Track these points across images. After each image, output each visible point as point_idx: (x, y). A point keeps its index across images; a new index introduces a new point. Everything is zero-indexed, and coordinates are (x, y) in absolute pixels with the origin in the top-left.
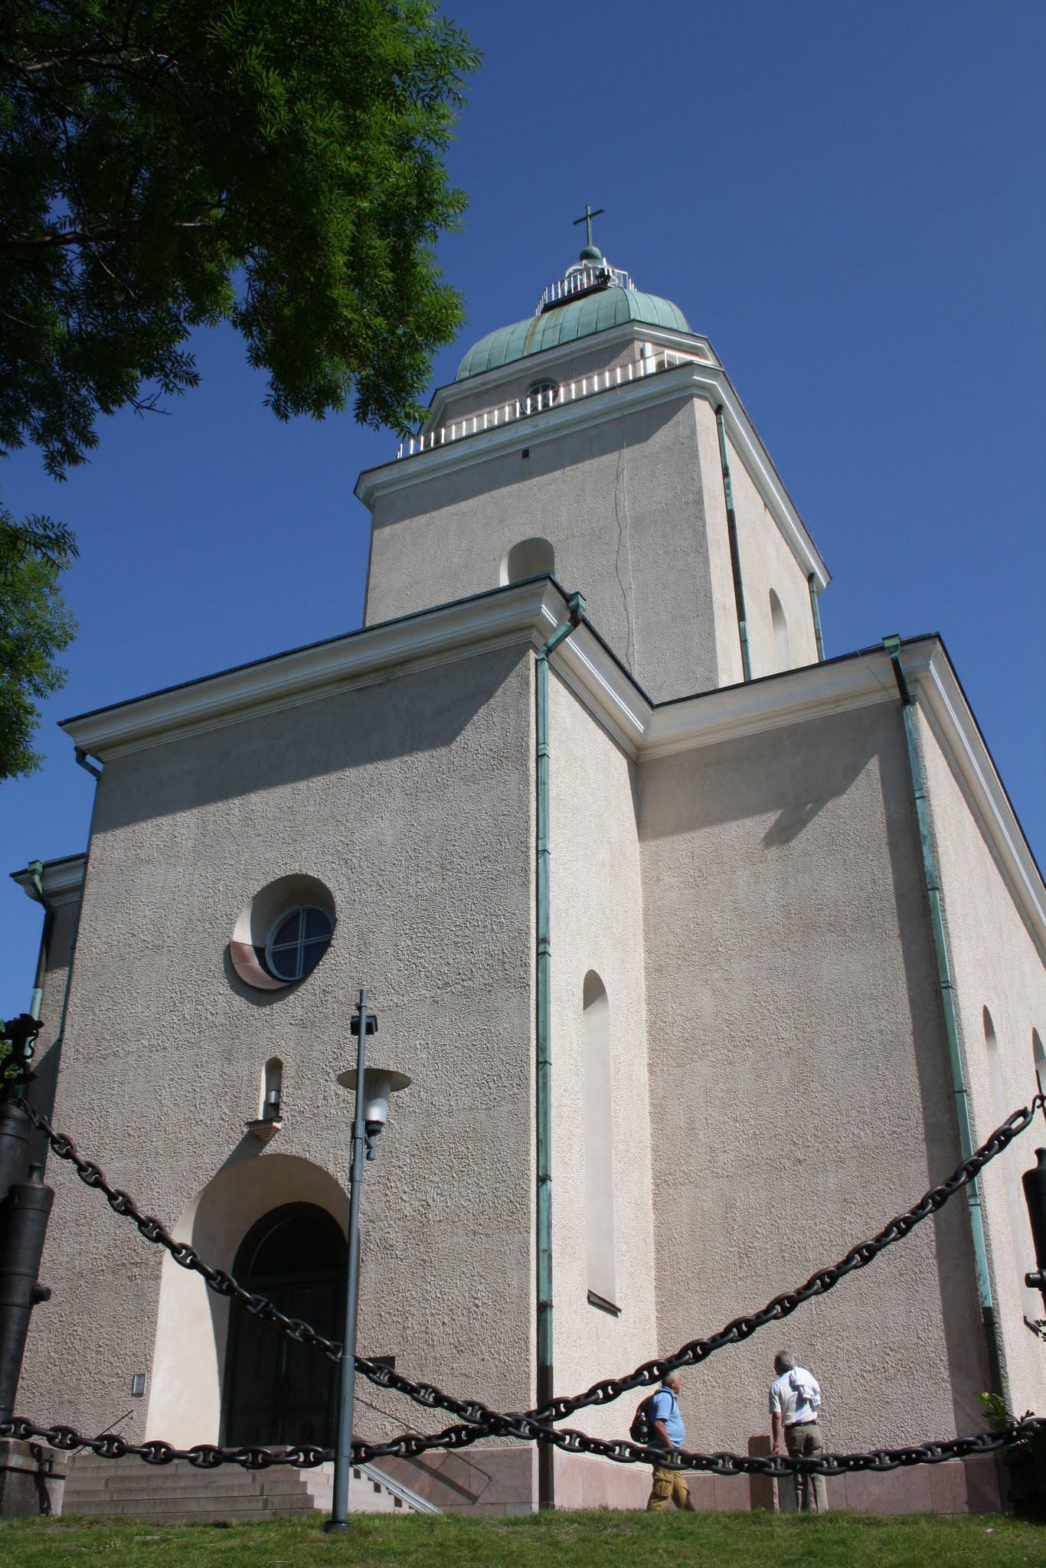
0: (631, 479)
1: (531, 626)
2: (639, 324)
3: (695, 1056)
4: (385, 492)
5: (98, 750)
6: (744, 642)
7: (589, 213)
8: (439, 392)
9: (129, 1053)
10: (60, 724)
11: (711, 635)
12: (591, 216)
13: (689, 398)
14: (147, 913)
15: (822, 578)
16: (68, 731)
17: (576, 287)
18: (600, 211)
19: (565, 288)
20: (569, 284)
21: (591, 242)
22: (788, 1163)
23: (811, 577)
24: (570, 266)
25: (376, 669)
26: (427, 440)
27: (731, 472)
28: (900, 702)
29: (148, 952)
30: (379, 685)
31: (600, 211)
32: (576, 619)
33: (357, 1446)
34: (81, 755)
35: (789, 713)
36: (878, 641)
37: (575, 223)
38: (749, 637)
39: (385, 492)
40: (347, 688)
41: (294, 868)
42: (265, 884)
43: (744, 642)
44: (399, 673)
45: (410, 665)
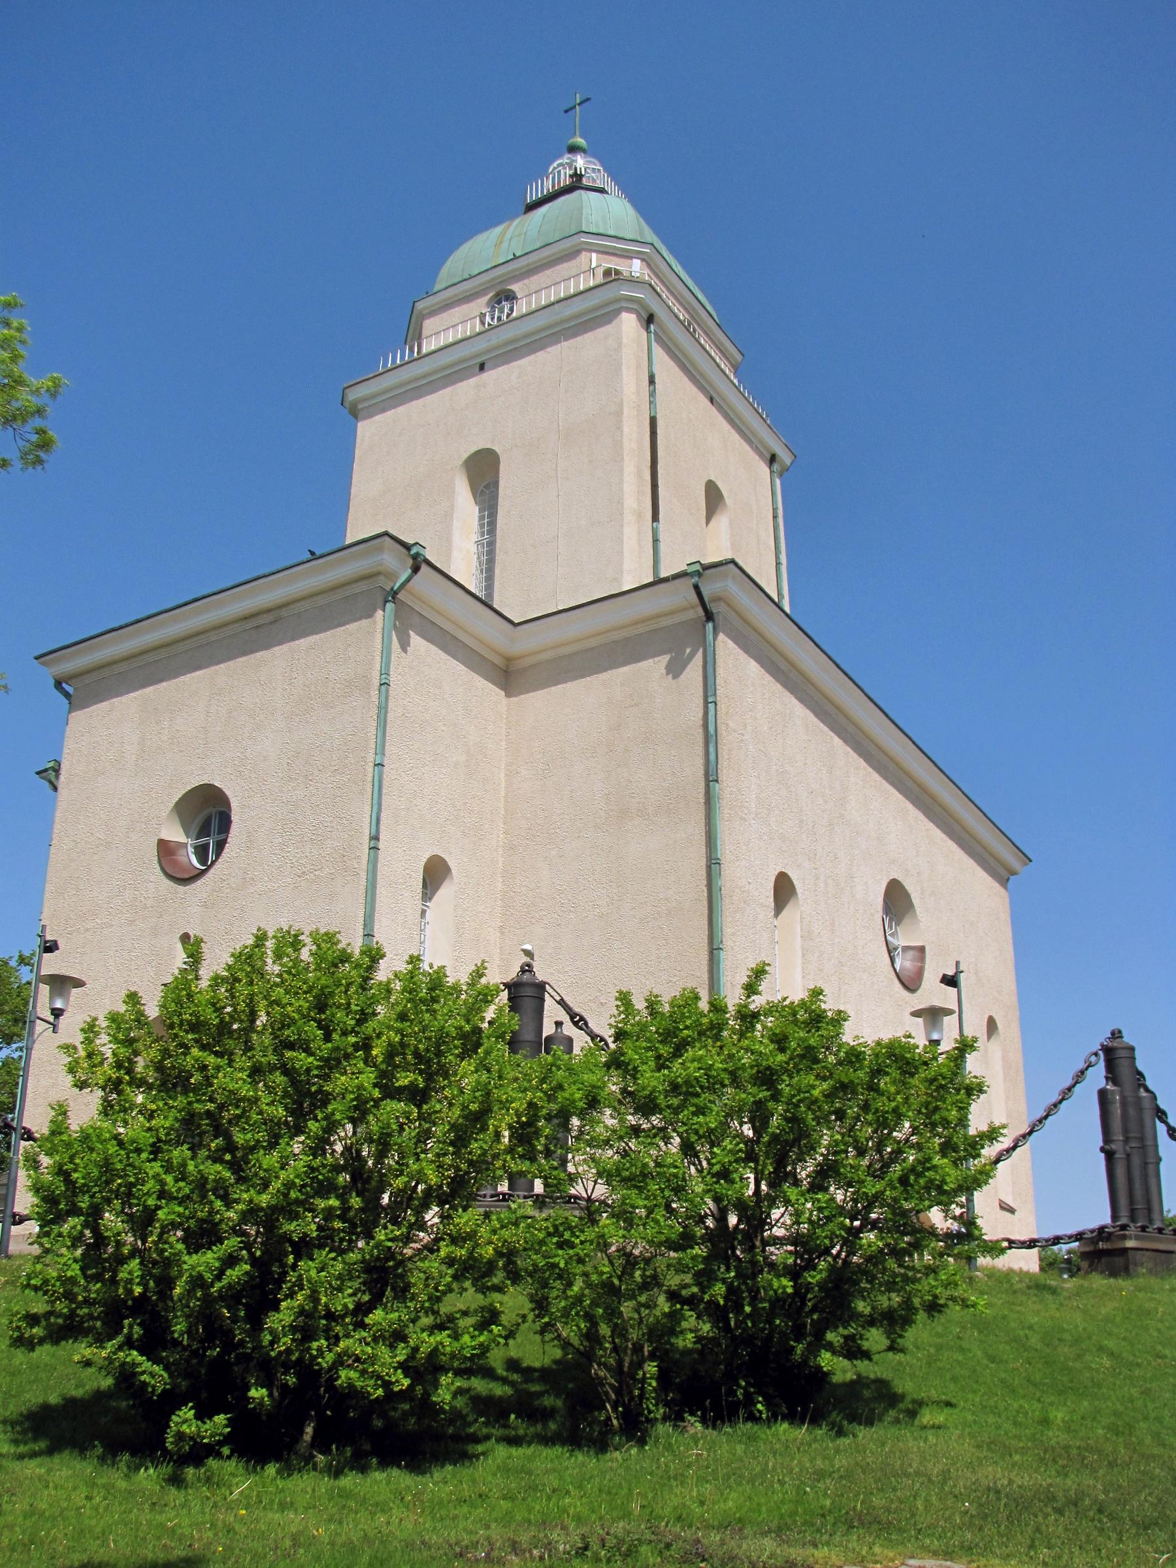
0: (566, 392)
1: (378, 574)
2: (586, 235)
3: (533, 920)
4: (366, 404)
5: (71, 678)
6: (656, 541)
7: (578, 101)
8: (416, 304)
9: (87, 930)
10: (36, 658)
11: (620, 540)
12: (579, 104)
13: (617, 312)
14: (102, 816)
15: (785, 457)
16: (43, 664)
17: (553, 186)
18: (588, 99)
19: (548, 186)
20: (553, 178)
21: (578, 133)
22: (594, 1006)
23: (772, 459)
24: (555, 161)
25: (269, 611)
26: (411, 350)
27: (657, 380)
28: (704, 619)
29: (101, 848)
30: (271, 623)
31: (588, 99)
32: (418, 563)
33: (14, 1215)
34: (58, 684)
35: (597, 635)
36: (683, 567)
37: (566, 111)
38: (661, 538)
39: (366, 404)
40: (249, 624)
41: (205, 780)
42: (184, 792)
43: (656, 541)
44: (284, 613)
45: (292, 606)
